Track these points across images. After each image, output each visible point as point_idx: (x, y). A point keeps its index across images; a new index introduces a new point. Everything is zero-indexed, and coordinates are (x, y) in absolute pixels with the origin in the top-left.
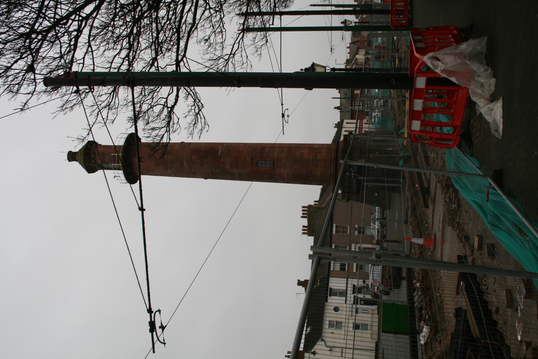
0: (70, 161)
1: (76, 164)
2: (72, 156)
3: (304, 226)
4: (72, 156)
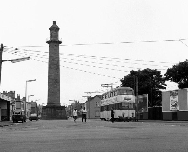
0: (53, 22)
1: (52, 24)
2: (54, 23)
3: (6, 91)
4: (54, 23)
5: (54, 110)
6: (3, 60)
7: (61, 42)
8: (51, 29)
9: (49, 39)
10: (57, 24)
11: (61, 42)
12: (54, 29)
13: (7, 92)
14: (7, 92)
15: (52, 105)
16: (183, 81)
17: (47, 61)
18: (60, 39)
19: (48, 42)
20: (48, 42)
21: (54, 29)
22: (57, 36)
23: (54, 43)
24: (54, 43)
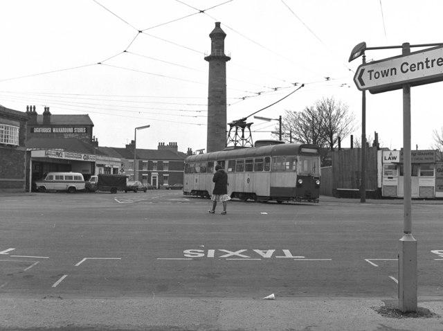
1: (214, 27)
2: (218, 24)
4: (218, 24)
5: (406, 86)
6: (349, 146)
7: (229, 59)
8: (211, 35)
9: (209, 53)
10: (222, 27)
11: (229, 59)
12: (218, 36)
13: (165, 145)
14: (165, 145)
15: (401, 265)
16: (211, 253)
17: (205, 121)
18: (227, 54)
19: (207, 59)
20: (207, 59)
21: (218, 36)
22: (222, 47)
23: (218, 60)
24: (218, 60)
